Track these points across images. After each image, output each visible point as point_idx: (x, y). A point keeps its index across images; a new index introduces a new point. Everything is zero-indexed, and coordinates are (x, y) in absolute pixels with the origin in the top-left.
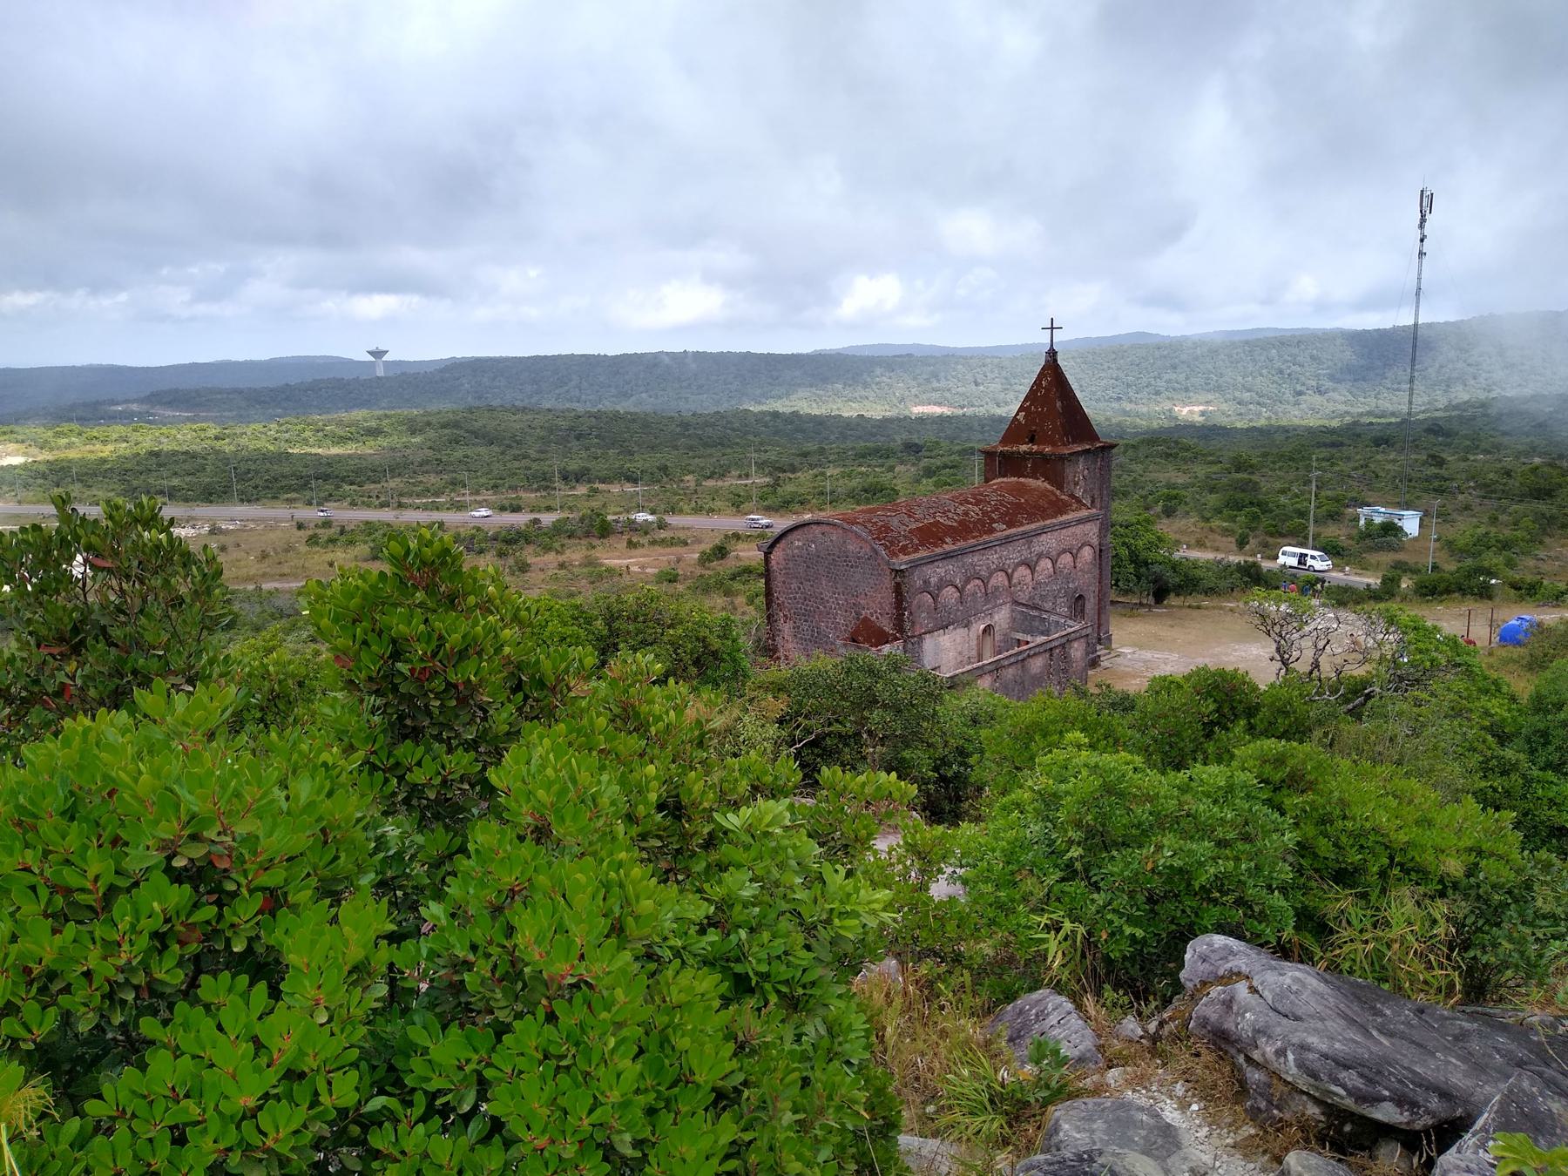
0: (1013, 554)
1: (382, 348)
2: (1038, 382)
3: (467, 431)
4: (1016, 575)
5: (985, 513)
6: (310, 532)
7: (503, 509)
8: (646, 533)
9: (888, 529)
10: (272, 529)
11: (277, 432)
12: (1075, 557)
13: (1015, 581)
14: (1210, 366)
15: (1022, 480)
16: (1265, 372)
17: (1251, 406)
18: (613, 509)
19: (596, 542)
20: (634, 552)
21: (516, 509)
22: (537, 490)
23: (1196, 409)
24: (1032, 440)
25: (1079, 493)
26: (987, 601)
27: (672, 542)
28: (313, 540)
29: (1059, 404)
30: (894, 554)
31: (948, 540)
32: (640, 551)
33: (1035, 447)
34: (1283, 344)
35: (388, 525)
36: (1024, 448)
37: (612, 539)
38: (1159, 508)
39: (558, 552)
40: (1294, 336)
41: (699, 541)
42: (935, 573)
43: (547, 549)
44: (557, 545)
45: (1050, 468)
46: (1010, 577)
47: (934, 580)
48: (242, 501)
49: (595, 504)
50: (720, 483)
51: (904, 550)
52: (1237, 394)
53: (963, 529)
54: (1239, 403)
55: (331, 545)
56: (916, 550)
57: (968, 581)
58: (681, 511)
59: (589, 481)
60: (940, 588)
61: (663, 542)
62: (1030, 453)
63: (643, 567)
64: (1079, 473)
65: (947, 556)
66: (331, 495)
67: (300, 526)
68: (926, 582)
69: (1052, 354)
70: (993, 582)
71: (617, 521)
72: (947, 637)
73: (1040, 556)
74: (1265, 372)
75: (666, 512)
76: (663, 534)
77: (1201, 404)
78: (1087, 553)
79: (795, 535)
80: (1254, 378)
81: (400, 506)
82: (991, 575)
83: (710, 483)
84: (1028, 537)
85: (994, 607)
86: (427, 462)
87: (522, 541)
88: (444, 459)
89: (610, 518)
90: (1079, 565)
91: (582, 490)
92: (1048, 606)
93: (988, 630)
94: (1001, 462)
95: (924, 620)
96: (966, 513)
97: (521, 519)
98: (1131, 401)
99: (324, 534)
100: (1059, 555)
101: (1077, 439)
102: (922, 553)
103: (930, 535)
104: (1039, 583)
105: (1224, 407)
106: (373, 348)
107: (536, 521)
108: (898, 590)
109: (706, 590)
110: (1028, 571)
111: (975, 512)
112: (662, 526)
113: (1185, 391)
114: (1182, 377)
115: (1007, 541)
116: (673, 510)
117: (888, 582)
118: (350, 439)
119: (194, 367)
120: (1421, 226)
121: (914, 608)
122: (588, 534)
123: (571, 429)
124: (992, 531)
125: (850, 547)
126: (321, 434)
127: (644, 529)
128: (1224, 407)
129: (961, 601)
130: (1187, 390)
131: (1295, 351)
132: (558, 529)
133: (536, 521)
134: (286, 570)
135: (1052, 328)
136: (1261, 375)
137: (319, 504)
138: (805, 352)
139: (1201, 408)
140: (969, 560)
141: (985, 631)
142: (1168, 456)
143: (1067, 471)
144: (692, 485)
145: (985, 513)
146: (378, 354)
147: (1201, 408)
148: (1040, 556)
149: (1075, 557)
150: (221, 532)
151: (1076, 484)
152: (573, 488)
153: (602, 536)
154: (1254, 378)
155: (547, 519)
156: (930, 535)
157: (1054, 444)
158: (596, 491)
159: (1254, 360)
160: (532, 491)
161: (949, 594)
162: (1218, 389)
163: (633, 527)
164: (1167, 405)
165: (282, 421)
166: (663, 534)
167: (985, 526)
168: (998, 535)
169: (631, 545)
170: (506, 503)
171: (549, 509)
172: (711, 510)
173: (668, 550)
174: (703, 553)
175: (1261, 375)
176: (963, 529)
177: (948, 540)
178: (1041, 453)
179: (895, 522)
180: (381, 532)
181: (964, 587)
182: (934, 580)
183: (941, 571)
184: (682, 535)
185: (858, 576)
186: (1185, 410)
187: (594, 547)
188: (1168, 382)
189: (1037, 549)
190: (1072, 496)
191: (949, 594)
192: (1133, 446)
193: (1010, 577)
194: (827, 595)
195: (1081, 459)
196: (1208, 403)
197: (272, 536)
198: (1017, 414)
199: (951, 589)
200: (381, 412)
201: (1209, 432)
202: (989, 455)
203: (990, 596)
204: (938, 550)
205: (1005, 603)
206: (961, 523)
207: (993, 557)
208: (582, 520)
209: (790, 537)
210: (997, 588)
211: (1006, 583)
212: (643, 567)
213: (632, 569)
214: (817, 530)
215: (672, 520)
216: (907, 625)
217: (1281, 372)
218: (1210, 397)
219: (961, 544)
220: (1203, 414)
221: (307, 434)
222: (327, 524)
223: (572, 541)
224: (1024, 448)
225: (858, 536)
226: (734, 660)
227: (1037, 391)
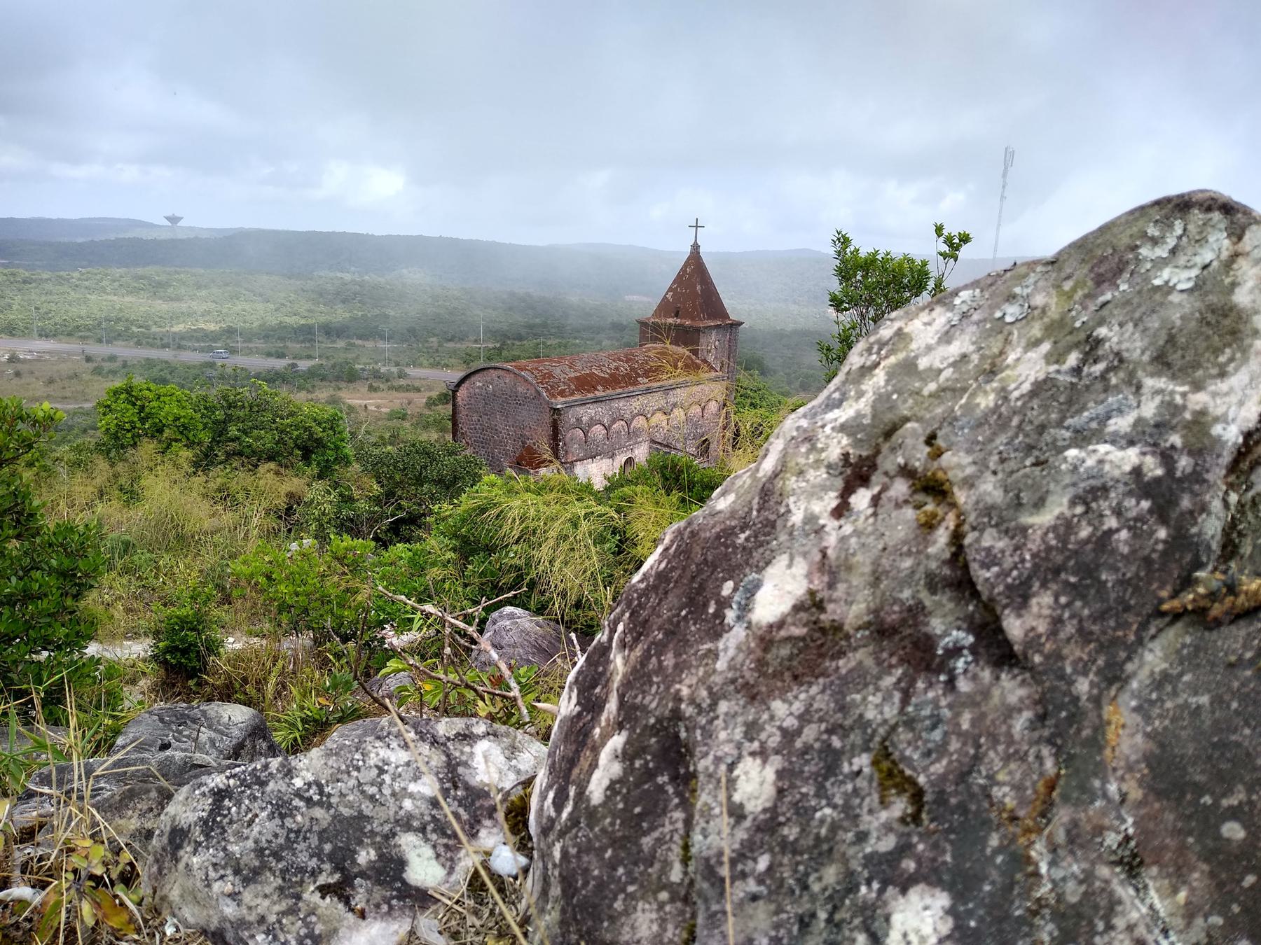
0: (655, 401)
1: (178, 215)
2: (683, 269)
5: (632, 369)
6: (95, 365)
7: (269, 355)
8: (387, 381)
9: (550, 375)
10: (64, 361)
11: (79, 279)
18: (364, 360)
19: (343, 385)
20: (374, 395)
21: (281, 356)
22: (303, 342)
24: (677, 315)
25: (710, 359)
26: (629, 439)
27: (408, 389)
28: (97, 371)
29: (698, 287)
30: (554, 396)
31: (599, 388)
32: (379, 394)
35: (166, 362)
36: (670, 320)
37: (357, 384)
38: (797, 384)
39: (308, 391)
41: (430, 389)
42: (587, 413)
43: (300, 388)
44: (309, 386)
45: (687, 337)
47: (585, 419)
48: (41, 336)
49: (350, 356)
50: (458, 345)
51: (562, 394)
53: (613, 381)
55: (111, 376)
56: (572, 394)
57: (614, 421)
58: (421, 365)
59: (348, 337)
60: (590, 425)
61: (399, 389)
63: (378, 407)
64: (711, 343)
65: (597, 401)
66: (119, 335)
67: (88, 359)
69: (696, 247)
70: (634, 423)
71: (363, 370)
73: (675, 405)
75: (408, 365)
76: (402, 382)
78: (713, 406)
79: (477, 377)
81: (180, 347)
82: (633, 418)
83: (451, 345)
84: (668, 390)
86: (209, 313)
87: (280, 380)
88: (224, 311)
89: (357, 367)
91: (341, 344)
92: (680, 446)
93: (629, 461)
94: (650, 331)
95: (575, 450)
96: (617, 368)
97: (280, 364)
99: (107, 366)
101: (712, 316)
102: (577, 397)
103: (585, 384)
106: (169, 214)
107: (294, 365)
108: (555, 427)
109: (426, 427)
111: (624, 368)
112: (401, 375)
115: (648, 391)
116: (415, 364)
117: (547, 419)
120: (1004, 175)
121: (567, 440)
122: (338, 378)
123: (338, 294)
124: (636, 383)
125: (520, 389)
126: (117, 284)
127: (387, 378)
132: (312, 374)
133: (294, 365)
134: (68, 394)
137: (108, 342)
138: (540, 244)
140: (615, 404)
141: (626, 462)
144: (435, 345)
145: (632, 369)
146: (174, 220)
148: (675, 405)
150: (19, 360)
151: (709, 351)
152: (333, 342)
153: (350, 381)
155: (304, 365)
156: (585, 384)
157: (693, 319)
158: (353, 345)
160: (298, 342)
161: (598, 431)
163: (377, 375)
165: (84, 270)
166: (402, 382)
167: (631, 379)
168: (640, 387)
169: (372, 389)
170: (273, 350)
171: (309, 357)
172: (447, 366)
173: (403, 395)
174: (430, 398)
176: (613, 381)
177: (599, 388)
179: (557, 371)
180: (159, 368)
181: (610, 426)
182: (585, 419)
183: (592, 412)
184: (417, 384)
185: (525, 413)
187: (340, 389)
189: (672, 400)
190: (705, 361)
191: (598, 431)
194: (500, 427)
195: (714, 333)
197: (63, 366)
199: (599, 427)
200: (172, 269)
202: (643, 324)
203: (632, 435)
204: (590, 395)
206: (611, 375)
207: (636, 404)
208: (334, 366)
209: (473, 379)
210: (637, 429)
212: (378, 407)
213: (370, 408)
214: (494, 373)
215: (411, 371)
216: (562, 453)
219: (610, 392)
221: (105, 283)
222: (112, 358)
223: (324, 383)
224: (670, 320)
225: (526, 380)
226: (337, 448)
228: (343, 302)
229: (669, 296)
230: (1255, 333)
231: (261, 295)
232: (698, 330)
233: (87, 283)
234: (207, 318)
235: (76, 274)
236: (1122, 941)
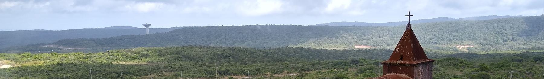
1: (148, 23)
3: (182, 55)
14: (471, 31)
15: (398, 74)
16: (492, 32)
17: (487, 46)
23: (465, 47)
24: (401, 59)
29: (412, 45)
33: (403, 62)
34: (499, 22)
36: (398, 62)
40: (503, 19)
50: (280, 76)
52: (481, 41)
54: (482, 45)
59: (229, 75)
62: (401, 64)
69: (409, 25)
74: (492, 32)
77: (467, 45)
80: (488, 35)
88: (173, 66)
98: (440, 44)
105: (476, 46)
106: (145, 23)
113: (461, 40)
114: (460, 35)
118: (136, 58)
123: (222, 55)
126: (125, 56)
128: (476, 46)
130: (462, 39)
131: (504, 24)
135: (409, 16)
136: (491, 34)
139: (467, 46)
142: (454, 65)
143: (415, 71)
144: (269, 76)
146: (147, 25)
147: (467, 46)
154: (488, 35)
157: (410, 61)
159: (488, 28)
162: (474, 39)
164: (454, 45)
175: (491, 34)
178: (405, 64)
186: (461, 47)
188: (455, 36)
192: (441, 61)
195: (421, 66)
196: (470, 44)
198: (396, 49)
201: (470, 56)
202: (385, 65)
217: (498, 32)
218: (471, 42)
220: (468, 49)
221: (119, 56)
224: (398, 62)
227: (403, 40)
228: (225, 58)
229: (397, 50)
230: (147, 23)
231: (188, 58)
232: (413, 66)
233: (112, 57)
234: (165, 70)
235: (106, 53)
236: (200, 77)
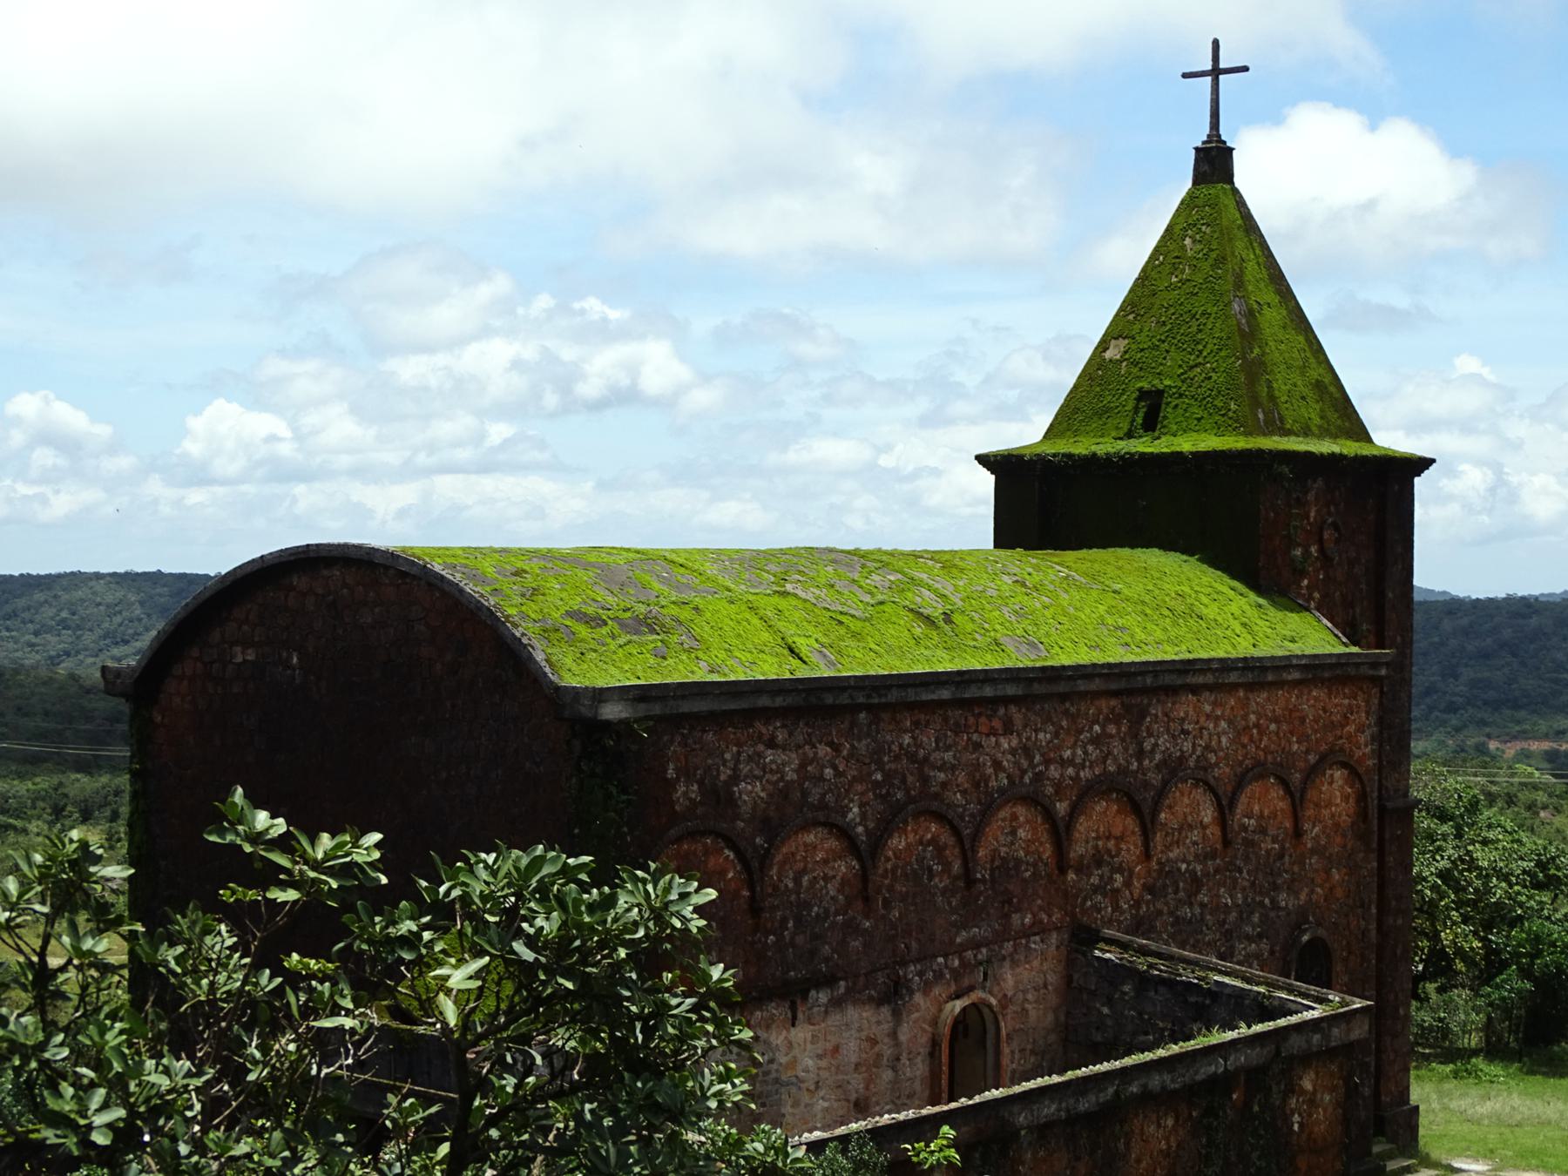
4: (1084, 827)
12: (1297, 800)
13: (1079, 850)
46: (1060, 833)
47: (751, 792)
68: (721, 799)
70: (994, 841)
72: (801, 1033)
73: (1174, 769)
77: (1546, 737)
82: (988, 811)
85: (1002, 936)
90: (1313, 831)
100: (1240, 784)
104: (1168, 872)
110: (1131, 823)
119: (346, 546)
129: (863, 890)
135: (1216, 72)
139: (1546, 745)
147: (1546, 745)
149: (1297, 800)
182: (751, 792)
183: (787, 763)
189: (1162, 743)
193: (1060, 833)
205: (1040, 929)
210: (1005, 868)
211: (1047, 851)
